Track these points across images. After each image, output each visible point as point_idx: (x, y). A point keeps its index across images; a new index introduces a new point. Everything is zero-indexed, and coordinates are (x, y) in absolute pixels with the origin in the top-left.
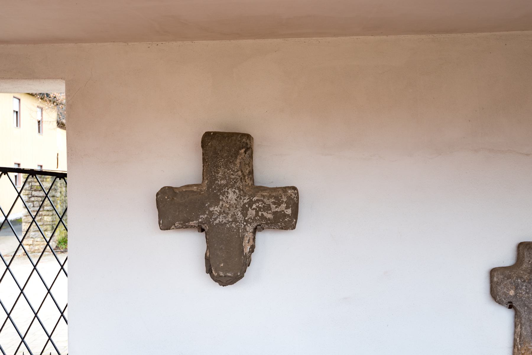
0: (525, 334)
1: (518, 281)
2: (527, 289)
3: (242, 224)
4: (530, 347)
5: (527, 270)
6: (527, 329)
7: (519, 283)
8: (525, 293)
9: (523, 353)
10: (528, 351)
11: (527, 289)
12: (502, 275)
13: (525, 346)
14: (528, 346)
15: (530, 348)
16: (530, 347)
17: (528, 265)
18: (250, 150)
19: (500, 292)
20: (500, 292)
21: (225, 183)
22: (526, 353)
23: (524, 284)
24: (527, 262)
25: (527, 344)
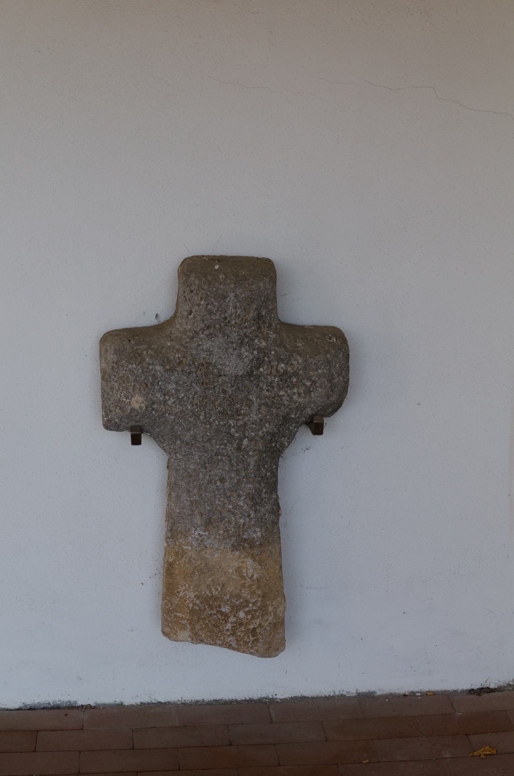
0: (178, 511)
1: (156, 371)
2: (179, 391)
3: (238, 532)
4: (188, 546)
5: (184, 337)
6: (182, 499)
7: (159, 373)
8: (174, 402)
9: (170, 563)
10: (182, 556)
11: (179, 391)
12: (260, 282)
13: (177, 543)
14: (183, 543)
15: (187, 549)
16: (187, 547)
17: (187, 323)
18: (234, 645)
19: (110, 400)
20: (110, 400)
21: (210, 564)
22: (177, 563)
23: (173, 378)
24: (185, 314)
25: (181, 538)
